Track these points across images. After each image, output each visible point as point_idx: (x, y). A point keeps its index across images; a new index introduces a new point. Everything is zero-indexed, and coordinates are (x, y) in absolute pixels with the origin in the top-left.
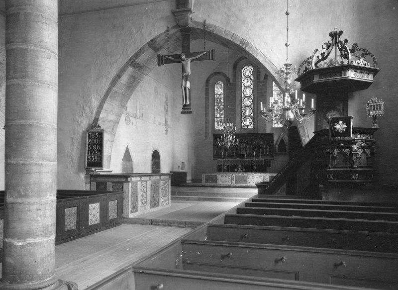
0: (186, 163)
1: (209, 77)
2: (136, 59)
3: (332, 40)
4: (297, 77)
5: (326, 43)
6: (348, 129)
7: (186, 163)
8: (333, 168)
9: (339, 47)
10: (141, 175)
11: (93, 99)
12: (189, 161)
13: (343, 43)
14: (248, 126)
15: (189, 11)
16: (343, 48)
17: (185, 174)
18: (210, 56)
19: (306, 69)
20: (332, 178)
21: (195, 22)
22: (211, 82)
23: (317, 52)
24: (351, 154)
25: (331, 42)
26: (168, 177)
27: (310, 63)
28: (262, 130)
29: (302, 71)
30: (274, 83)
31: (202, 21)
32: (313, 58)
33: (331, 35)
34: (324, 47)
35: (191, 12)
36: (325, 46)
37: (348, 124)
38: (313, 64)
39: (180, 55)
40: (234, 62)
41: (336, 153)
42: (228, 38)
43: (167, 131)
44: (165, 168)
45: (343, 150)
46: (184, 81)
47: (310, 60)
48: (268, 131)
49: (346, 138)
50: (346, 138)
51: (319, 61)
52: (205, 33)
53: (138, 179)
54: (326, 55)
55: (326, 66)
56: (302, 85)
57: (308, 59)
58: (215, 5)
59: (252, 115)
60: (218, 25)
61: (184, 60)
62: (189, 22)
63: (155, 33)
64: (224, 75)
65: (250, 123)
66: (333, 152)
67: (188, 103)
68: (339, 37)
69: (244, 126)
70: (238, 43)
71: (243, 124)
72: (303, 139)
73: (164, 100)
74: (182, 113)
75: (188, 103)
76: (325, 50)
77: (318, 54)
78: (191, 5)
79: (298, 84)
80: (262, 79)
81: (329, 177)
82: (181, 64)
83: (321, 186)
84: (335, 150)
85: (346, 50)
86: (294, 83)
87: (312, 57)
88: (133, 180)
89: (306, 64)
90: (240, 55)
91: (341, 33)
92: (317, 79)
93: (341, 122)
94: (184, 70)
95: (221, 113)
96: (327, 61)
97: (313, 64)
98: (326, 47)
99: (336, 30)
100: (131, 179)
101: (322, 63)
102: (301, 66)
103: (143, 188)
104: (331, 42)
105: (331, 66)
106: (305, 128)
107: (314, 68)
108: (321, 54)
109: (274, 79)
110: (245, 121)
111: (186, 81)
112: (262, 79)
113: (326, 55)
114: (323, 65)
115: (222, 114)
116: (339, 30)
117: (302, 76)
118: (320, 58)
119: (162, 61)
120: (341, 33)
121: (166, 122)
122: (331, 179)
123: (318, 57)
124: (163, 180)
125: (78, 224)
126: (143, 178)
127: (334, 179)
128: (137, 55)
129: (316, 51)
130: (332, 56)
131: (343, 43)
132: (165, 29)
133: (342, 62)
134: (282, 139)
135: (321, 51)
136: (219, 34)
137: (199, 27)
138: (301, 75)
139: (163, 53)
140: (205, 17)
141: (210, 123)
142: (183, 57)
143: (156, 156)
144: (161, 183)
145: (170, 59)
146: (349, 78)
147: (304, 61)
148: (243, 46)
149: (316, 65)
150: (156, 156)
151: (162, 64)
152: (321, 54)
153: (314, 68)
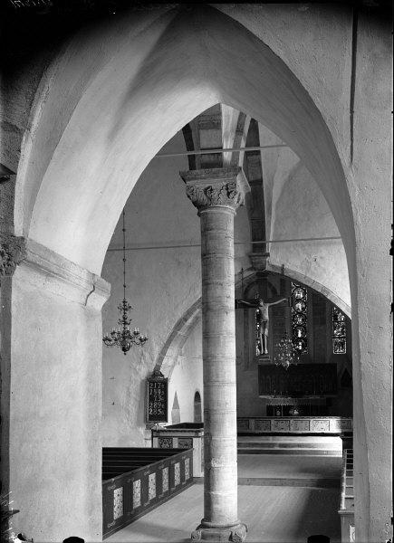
111: (264, 328)
142: (262, 304)
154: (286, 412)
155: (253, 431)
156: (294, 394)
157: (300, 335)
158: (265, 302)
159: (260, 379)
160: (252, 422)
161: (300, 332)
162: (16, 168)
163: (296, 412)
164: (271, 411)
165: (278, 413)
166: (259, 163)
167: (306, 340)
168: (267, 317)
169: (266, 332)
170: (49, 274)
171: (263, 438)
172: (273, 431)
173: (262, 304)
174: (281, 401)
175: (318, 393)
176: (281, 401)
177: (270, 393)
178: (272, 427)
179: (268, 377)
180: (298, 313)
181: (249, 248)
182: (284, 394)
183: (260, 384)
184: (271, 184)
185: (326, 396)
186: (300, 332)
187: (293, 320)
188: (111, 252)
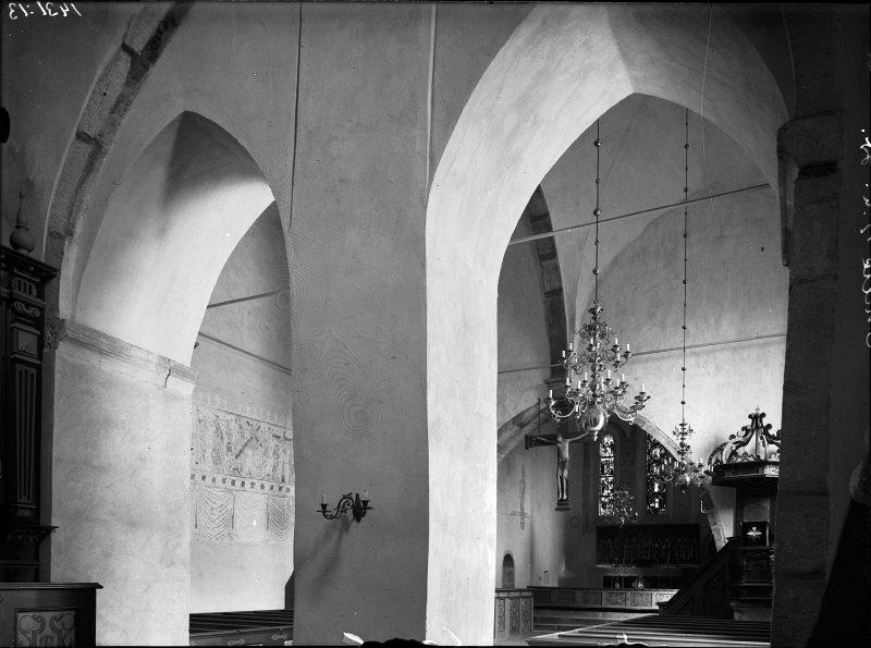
6: (764, 535)
11: (724, 527)
24: (768, 566)
32: (722, 450)
37: (764, 532)
39: (555, 438)
49: (761, 547)
50: (761, 547)
63: (522, 408)
67: (565, 497)
75: (565, 497)
91: (763, 415)
92: (729, 475)
93: (754, 529)
94: (559, 454)
106: (17, 356)
111: (563, 469)
116: (760, 412)
120: (763, 415)
124: (523, 598)
125: (735, 486)
132: (536, 401)
142: (560, 439)
154: (628, 583)
155: (580, 605)
156: (639, 563)
157: (656, 490)
158: (565, 437)
159: (598, 543)
160: (579, 594)
161: (657, 485)
162: (546, 209)
163: (640, 585)
164: (609, 583)
165: (618, 586)
166: (557, 268)
167: (664, 495)
168: (566, 455)
169: (566, 473)
170: (101, 352)
171: (591, 613)
172: (604, 605)
173: (560, 439)
174: (624, 571)
175: (673, 561)
176: (624, 571)
177: (611, 562)
178: (604, 601)
179: (609, 541)
180: (655, 461)
181: (549, 373)
182: (628, 563)
183: (598, 550)
184: (574, 292)
185: (683, 566)
186: (657, 485)
187: (649, 471)
188: (507, 375)
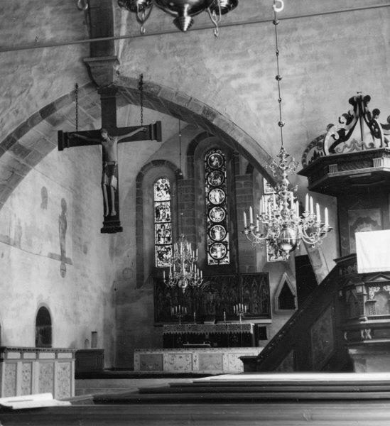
0: (100, 334)
1: (142, 169)
2: (19, 138)
3: (355, 110)
4: (300, 168)
5: (344, 115)
7: (100, 334)
8: (369, 318)
9: (366, 121)
10: (22, 350)
12: (107, 329)
13: (372, 115)
14: (219, 260)
15: (116, 60)
16: (372, 124)
17: (100, 352)
18: (153, 132)
19: (316, 155)
20: (370, 337)
21: (125, 79)
22: (146, 178)
23: (332, 129)
25: (352, 113)
26: (70, 355)
27: (322, 145)
28: (247, 267)
29: (309, 159)
30: (265, 181)
31: (136, 77)
33: (351, 101)
34: (342, 120)
35: (118, 63)
36: (344, 120)
38: (326, 148)
40: (190, 142)
41: (373, 294)
42: (183, 104)
43: (63, 271)
44: (63, 335)
45: (384, 287)
46: (106, 176)
47: (322, 141)
48: (259, 268)
51: (337, 143)
52: (144, 94)
53: (17, 355)
54: (347, 132)
55: (347, 151)
56: (311, 182)
57: (318, 139)
58: (157, 51)
59: (227, 239)
60: (165, 84)
61: (105, 140)
62: (115, 78)
64: (171, 166)
65: (222, 254)
66: (368, 291)
68: (366, 106)
69: (211, 261)
70: (200, 113)
71: (209, 258)
72: (317, 272)
73: (60, 211)
74: (103, 231)
75: (114, 213)
76: (344, 126)
77: (333, 131)
78: (118, 52)
79: (305, 180)
80: (243, 172)
81: (365, 334)
82: (101, 146)
83: (352, 351)
84: (371, 289)
85: (377, 126)
86: (298, 180)
87: (323, 137)
88: (9, 357)
89: (315, 149)
90: (200, 130)
92: (334, 173)
95: (167, 235)
96: (348, 142)
97: (326, 148)
98: (345, 121)
99: (360, 94)
100: (6, 356)
101: (341, 145)
102: (307, 151)
103: (26, 374)
104: (352, 113)
105: (355, 151)
107: (328, 154)
108: (338, 132)
109: (265, 174)
110: (214, 250)
112: (243, 172)
113: (347, 132)
114: (343, 149)
115: (169, 238)
116: (364, 95)
117: (309, 166)
118: (337, 137)
119: (66, 141)
120: (368, 98)
121: (63, 252)
122: (369, 339)
123: (333, 136)
126: (26, 355)
127: (373, 338)
128: (21, 131)
129: (330, 126)
130: (356, 134)
131: (372, 115)
132: (72, 88)
133: (372, 145)
134: (286, 284)
135: (337, 127)
136: (168, 98)
137: (131, 86)
138: (308, 164)
139: (68, 127)
140: (143, 69)
141: (175, 214)
142: (105, 135)
143: (43, 318)
144: (58, 367)
145: (80, 139)
146: (385, 170)
147: (312, 142)
148: (209, 118)
149: (331, 149)
150: (43, 318)
151: (67, 146)
152: (338, 132)
153: (328, 154)
